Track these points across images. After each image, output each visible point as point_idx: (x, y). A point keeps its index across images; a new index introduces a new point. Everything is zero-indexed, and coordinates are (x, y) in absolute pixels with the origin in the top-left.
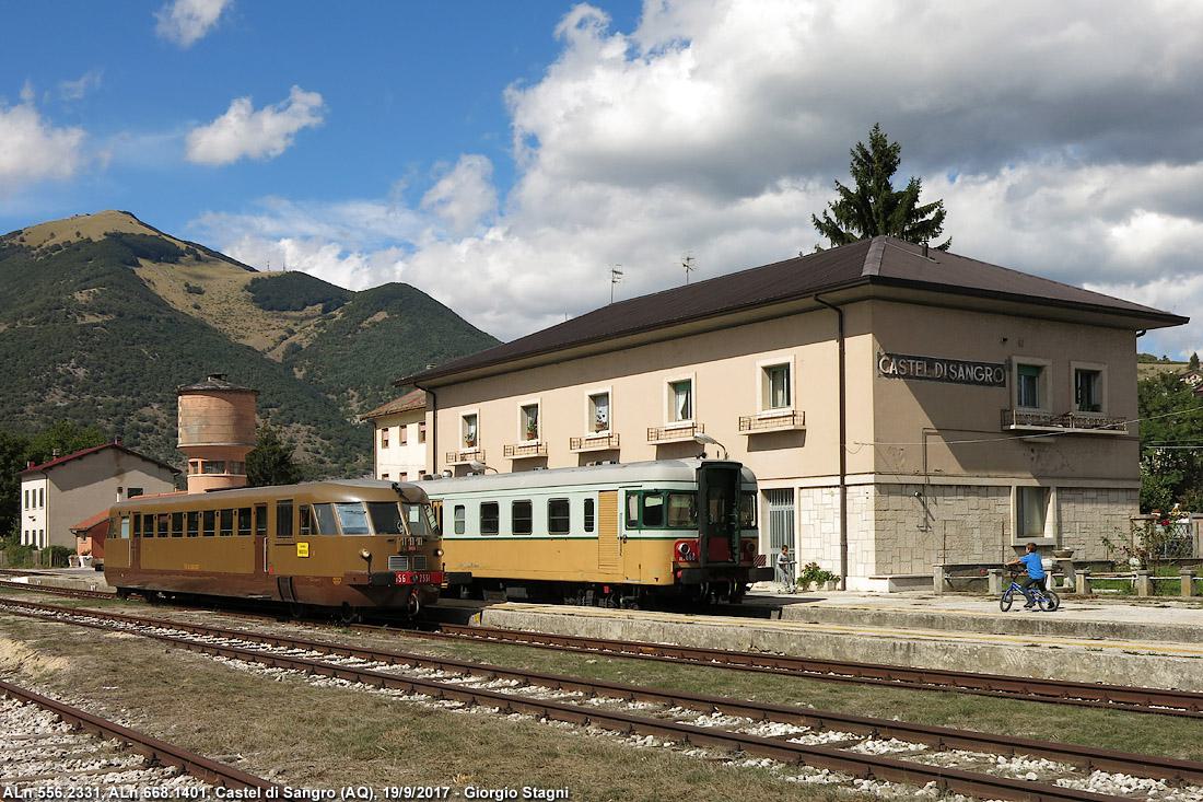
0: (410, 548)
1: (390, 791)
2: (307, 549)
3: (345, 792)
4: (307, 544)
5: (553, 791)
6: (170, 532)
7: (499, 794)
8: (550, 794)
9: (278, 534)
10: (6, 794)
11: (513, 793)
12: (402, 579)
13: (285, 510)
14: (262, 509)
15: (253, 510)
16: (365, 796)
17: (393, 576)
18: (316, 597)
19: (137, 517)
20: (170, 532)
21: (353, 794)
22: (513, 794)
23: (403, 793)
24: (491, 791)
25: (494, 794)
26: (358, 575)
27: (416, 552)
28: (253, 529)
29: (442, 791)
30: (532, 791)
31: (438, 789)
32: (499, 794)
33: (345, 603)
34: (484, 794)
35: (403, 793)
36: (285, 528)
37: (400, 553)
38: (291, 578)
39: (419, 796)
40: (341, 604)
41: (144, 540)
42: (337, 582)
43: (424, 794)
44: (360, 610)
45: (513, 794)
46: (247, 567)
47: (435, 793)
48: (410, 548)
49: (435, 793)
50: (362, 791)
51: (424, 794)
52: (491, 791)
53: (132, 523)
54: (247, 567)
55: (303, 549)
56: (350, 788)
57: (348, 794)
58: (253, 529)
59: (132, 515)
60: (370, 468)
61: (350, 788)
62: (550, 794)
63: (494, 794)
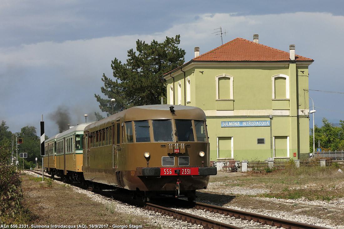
1: (91, 225)
3: (78, 226)
7: (122, 227)
8: (137, 227)
10: (1, 227)
16: (84, 227)
22: (126, 227)
23: (95, 226)
24: (120, 226)
25: (121, 227)
29: (106, 226)
30: (34, 226)
31: (105, 225)
32: (122, 227)
34: (43, 227)
35: (95, 226)
39: (99, 227)
45: (126, 227)
47: (104, 226)
48: (175, 151)
49: (104, 226)
50: (83, 226)
52: (120, 226)
57: (79, 227)
61: (80, 225)
62: (137, 227)
63: (121, 227)
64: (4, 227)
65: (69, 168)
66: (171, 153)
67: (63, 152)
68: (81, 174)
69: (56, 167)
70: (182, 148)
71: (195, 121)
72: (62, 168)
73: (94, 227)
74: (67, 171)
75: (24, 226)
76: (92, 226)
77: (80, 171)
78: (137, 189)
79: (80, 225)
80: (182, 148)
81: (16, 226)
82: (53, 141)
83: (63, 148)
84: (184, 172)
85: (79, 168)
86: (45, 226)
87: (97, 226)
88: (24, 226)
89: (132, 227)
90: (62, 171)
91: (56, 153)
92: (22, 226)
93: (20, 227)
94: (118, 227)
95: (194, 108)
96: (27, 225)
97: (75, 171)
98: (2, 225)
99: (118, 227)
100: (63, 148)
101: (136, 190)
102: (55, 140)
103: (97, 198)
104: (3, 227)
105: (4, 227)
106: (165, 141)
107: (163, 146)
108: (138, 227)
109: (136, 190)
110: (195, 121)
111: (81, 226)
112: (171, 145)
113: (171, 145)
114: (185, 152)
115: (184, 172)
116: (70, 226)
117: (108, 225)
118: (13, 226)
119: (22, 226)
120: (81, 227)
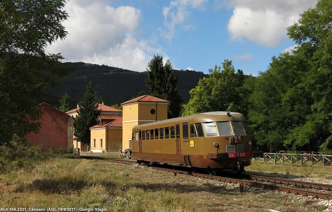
0: (235, 141)
1: (60, 209)
2: (193, 143)
3: (48, 210)
4: (193, 141)
5: (103, 209)
6: (164, 136)
7: (89, 210)
8: (102, 210)
9: (183, 137)
10: (1, 210)
12: (231, 156)
13: (185, 126)
14: (178, 127)
15: (175, 127)
16: (53, 210)
17: (226, 155)
18: (197, 164)
19: (140, 132)
20: (164, 136)
22: (44, 210)
23: (63, 210)
24: (87, 209)
25: (87, 210)
26: (213, 154)
27: (238, 143)
28: (175, 135)
29: (74, 209)
30: (97, 209)
31: (72, 209)
32: (89, 210)
33: (208, 167)
34: (85, 210)
35: (63, 210)
36: (186, 135)
37: (231, 144)
38: (189, 156)
39: (68, 210)
40: (207, 167)
41: (142, 141)
42: (205, 158)
43: (69, 210)
44: (214, 170)
45: (44, 210)
46: (174, 152)
48: (235, 141)
50: (53, 209)
51: (69, 210)
52: (87, 209)
53: (139, 134)
54: (174, 152)
55: (192, 142)
56: (49, 208)
57: (49, 210)
58: (175, 135)
59: (138, 131)
60: (75, 125)
61: (49, 208)
63: (87, 210)
64: (3, 210)
71: (242, 121)
78: (208, 167)
81: (15, 210)
84: (231, 156)
86: (41, 209)
87: (65, 210)
92: (20, 209)
93: (18, 210)
95: (94, 126)
96: (25, 209)
98: (2, 208)
105: (3, 210)
108: (103, 210)
110: (242, 121)
111: (51, 209)
115: (241, 155)
116: (103, 209)
118: (12, 209)
119: (20, 209)
120: (50, 210)
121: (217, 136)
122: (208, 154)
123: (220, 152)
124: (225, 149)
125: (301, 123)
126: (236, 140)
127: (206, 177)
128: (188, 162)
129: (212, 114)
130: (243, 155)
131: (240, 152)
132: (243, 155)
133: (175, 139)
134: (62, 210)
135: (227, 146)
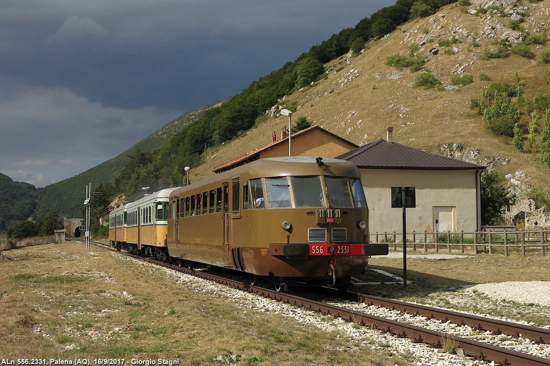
1: (97, 361)
5: (148, 361)
7: (147, 362)
8: (170, 362)
10: (3, 362)
11: (153, 362)
12: (318, 251)
16: (86, 363)
17: (306, 248)
21: (80, 362)
22: (154, 362)
23: (103, 362)
24: (144, 361)
25: (145, 362)
31: (119, 360)
32: (147, 362)
35: (103, 362)
39: (111, 363)
42: (264, 253)
44: (287, 279)
47: (118, 362)
48: (328, 220)
50: (85, 361)
52: (144, 361)
57: (78, 362)
61: (79, 360)
62: (170, 362)
63: (145, 362)
64: (82, 363)
65: (146, 241)
66: (322, 224)
67: (136, 223)
68: (164, 249)
69: (125, 241)
70: (337, 216)
72: (135, 242)
73: (101, 363)
74: (142, 245)
75: (39, 361)
76: (98, 362)
77: (163, 245)
78: (270, 273)
79: (79, 360)
80: (337, 216)
81: (26, 362)
82: (154, 201)
83: (136, 219)
85: (160, 243)
86: (65, 361)
88: (39, 361)
89: (162, 363)
90: (135, 246)
91: (125, 225)
92: (35, 361)
93: (32, 363)
94: (140, 362)
96: (44, 360)
97: (156, 245)
99: (140, 362)
100: (136, 219)
101: (268, 275)
102: (126, 210)
103: (210, 286)
104: (5, 362)
106: (310, 206)
107: (311, 213)
109: (268, 275)
112: (322, 211)
113: (322, 211)
114: (341, 222)
115: (341, 250)
117: (124, 360)
118: (21, 361)
119: (35, 361)
121: (289, 208)
122: (270, 246)
123: (295, 240)
124: (305, 235)
125: (239, 129)
126: (330, 217)
127: (266, 293)
128: (238, 264)
129: (286, 160)
130: (344, 251)
131: (338, 243)
132: (344, 251)
133: (221, 213)
134: (100, 362)
135: (312, 230)
